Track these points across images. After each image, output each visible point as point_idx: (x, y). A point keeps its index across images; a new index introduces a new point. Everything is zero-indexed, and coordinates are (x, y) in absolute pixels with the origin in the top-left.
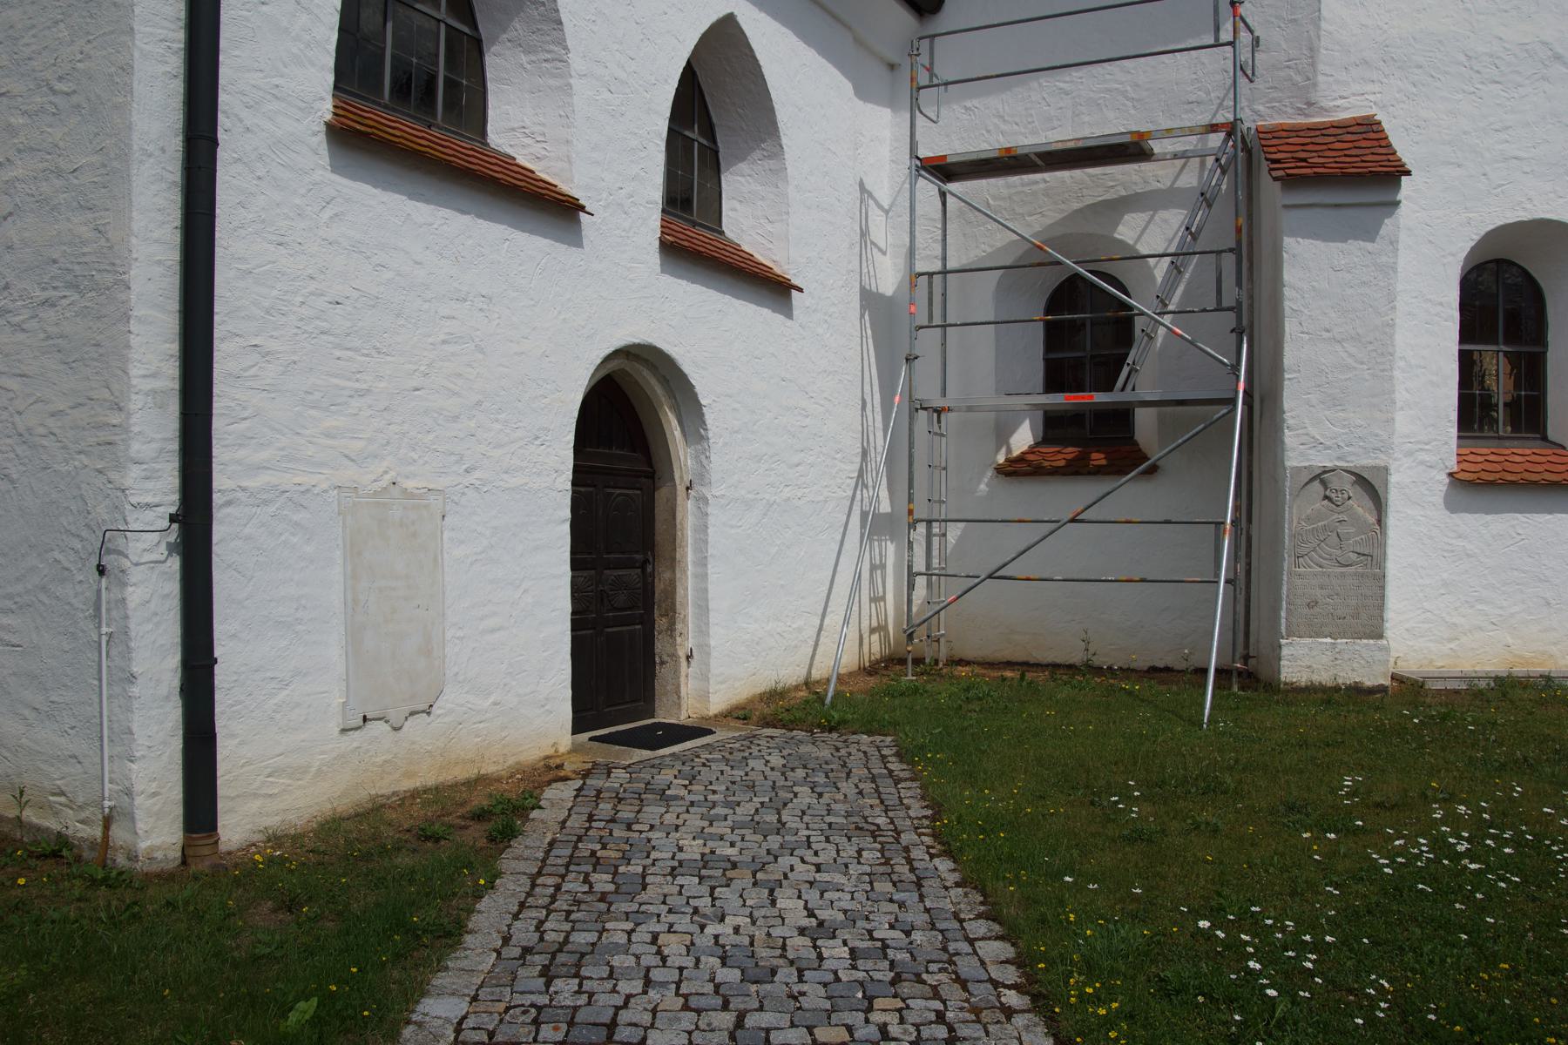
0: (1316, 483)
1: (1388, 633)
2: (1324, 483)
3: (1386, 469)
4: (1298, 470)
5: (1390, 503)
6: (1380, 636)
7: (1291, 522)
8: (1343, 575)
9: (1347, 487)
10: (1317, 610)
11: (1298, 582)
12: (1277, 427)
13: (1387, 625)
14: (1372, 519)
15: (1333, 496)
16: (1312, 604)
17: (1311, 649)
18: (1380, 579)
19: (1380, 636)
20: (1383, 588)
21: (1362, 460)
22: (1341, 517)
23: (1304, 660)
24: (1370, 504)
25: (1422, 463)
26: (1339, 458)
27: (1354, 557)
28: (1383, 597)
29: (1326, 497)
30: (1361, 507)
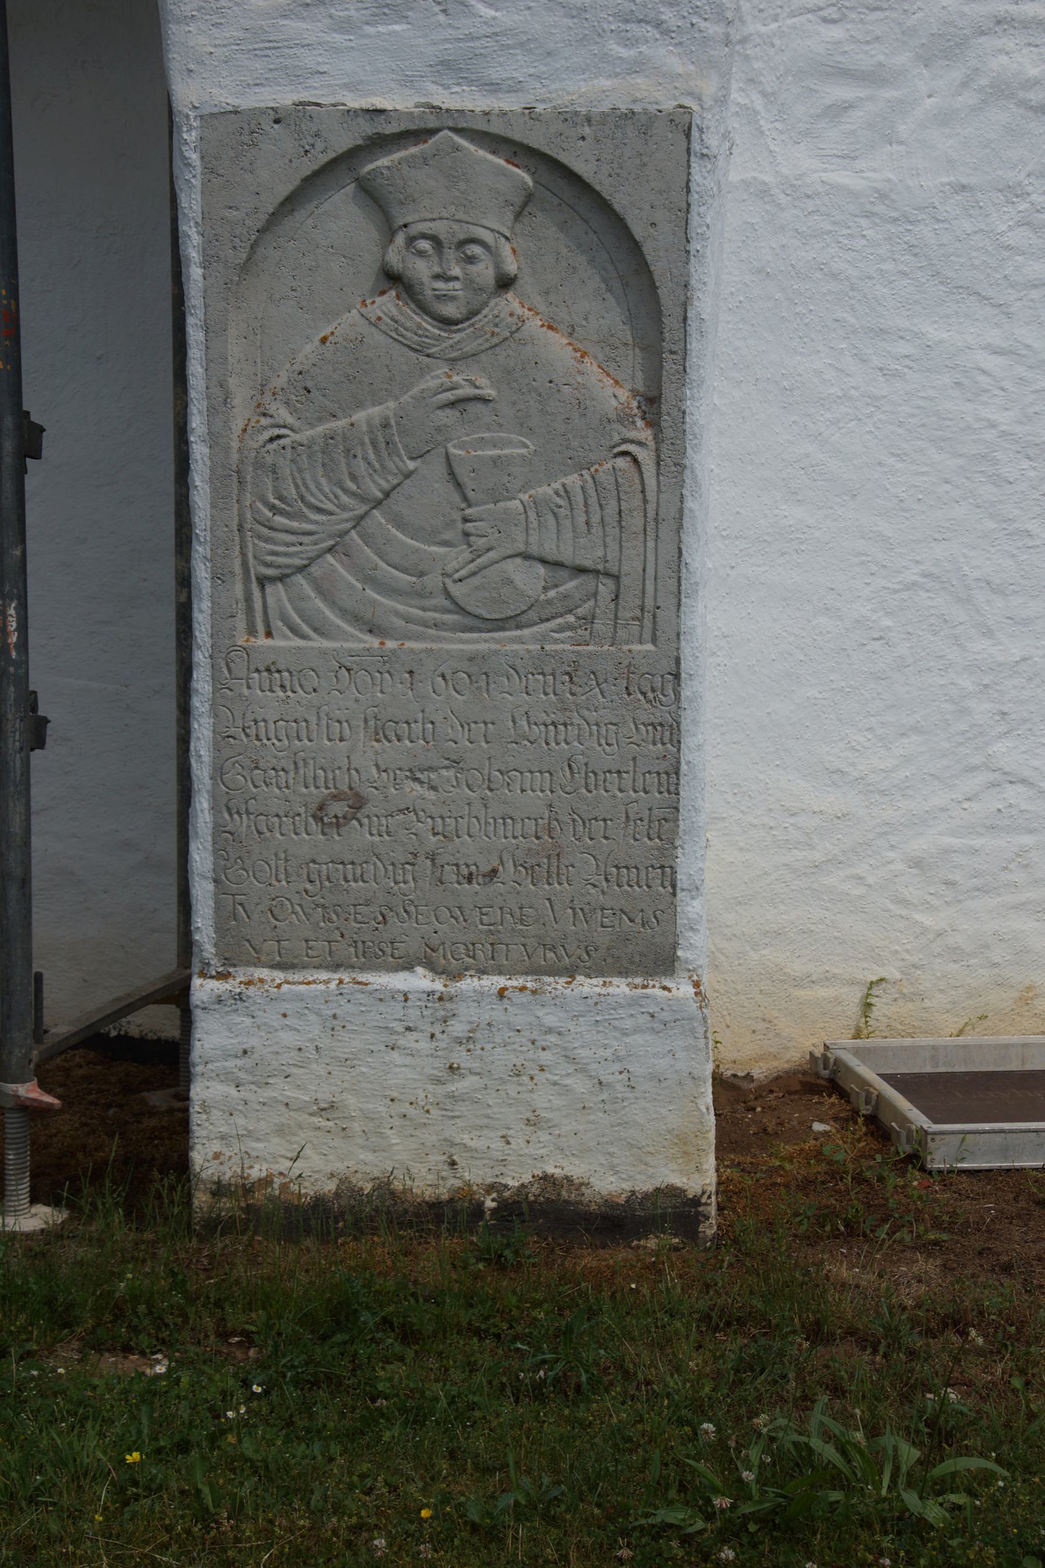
0: (340, 214)
1: (696, 947)
2: (373, 196)
3: (683, 126)
4: (243, 128)
5: (703, 305)
6: (662, 961)
7: (220, 405)
8: (479, 670)
9: (491, 223)
10: (360, 836)
11: (268, 703)
12: (178, 686)
13: (691, 908)
14: (612, 394)
15: (421, 270)
16: (341, 808)
17: (334, 1024)
18: (659, 691)
19: (662, 961)
20: (671, 732)
21: (563, 77)
22: (466, 380)
23: (312, 1085)
24: (606, 316)
25: (1002, 90)
26: (448, 68)
27: (528, 579)
28: (671, 775)
29: (393, 278)
30: (559, 333)
